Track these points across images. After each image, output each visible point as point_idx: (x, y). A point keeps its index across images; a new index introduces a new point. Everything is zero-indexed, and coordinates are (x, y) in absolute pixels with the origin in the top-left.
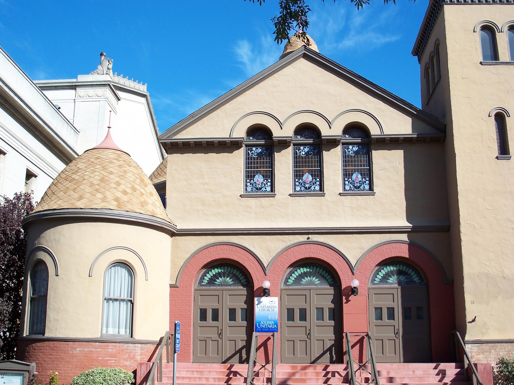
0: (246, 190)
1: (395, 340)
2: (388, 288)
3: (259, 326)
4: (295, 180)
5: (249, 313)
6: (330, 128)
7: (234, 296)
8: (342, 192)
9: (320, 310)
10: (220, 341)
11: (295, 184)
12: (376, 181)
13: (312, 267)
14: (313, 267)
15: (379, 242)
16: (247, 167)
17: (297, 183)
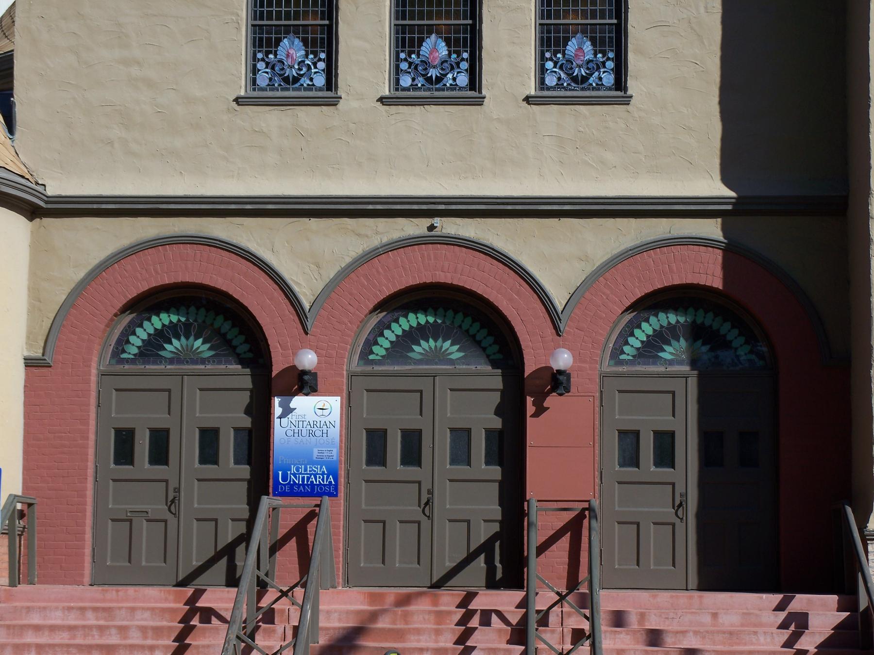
1: (674, 525)
2: (660, 376)
3: (285, 478)
4: (542, 54)
5: (257, 441)
7: (215, 394)
8: (533, 93)
9: (462, 437)
10: (172, 521)
11: (397, 67)
12: (633, 60)
13: (441, 311)
14: (446, 310)
15: (638, 242)
17: (404, 66)
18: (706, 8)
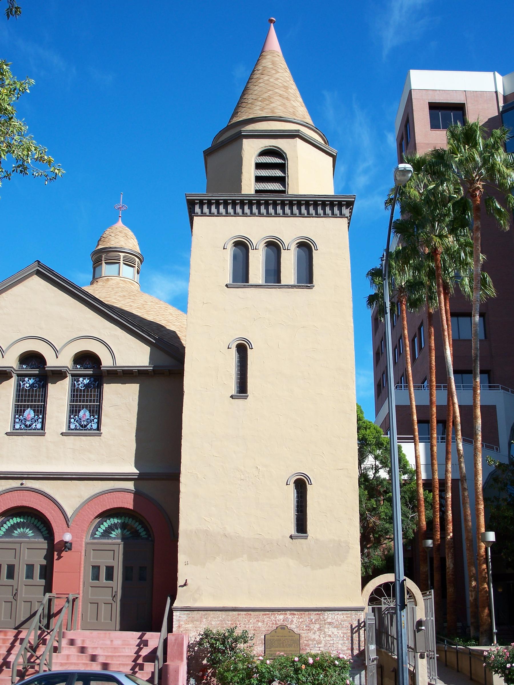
0: (69, 426)
4: (70, 416)
6: (57, 357)
9: (30, 568)
12: (104, 419)
15: (101, 490)
16: (72, 401)
17: (17, 420)
18: (132, 399)
